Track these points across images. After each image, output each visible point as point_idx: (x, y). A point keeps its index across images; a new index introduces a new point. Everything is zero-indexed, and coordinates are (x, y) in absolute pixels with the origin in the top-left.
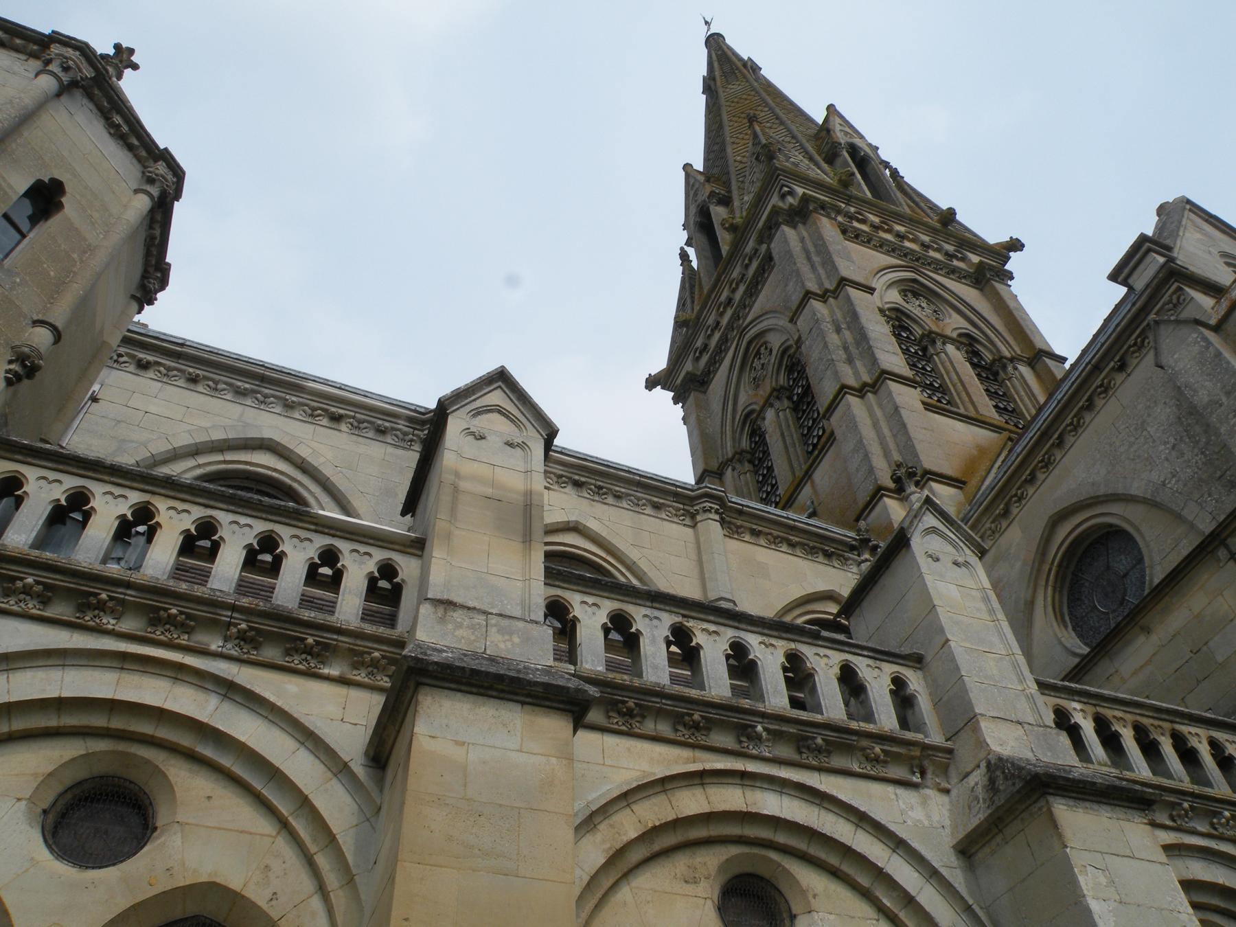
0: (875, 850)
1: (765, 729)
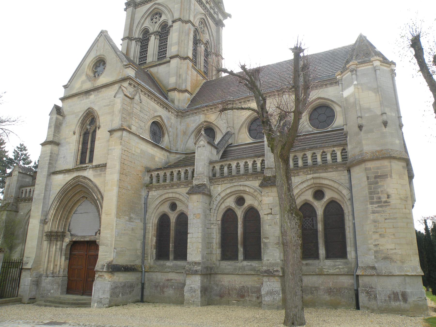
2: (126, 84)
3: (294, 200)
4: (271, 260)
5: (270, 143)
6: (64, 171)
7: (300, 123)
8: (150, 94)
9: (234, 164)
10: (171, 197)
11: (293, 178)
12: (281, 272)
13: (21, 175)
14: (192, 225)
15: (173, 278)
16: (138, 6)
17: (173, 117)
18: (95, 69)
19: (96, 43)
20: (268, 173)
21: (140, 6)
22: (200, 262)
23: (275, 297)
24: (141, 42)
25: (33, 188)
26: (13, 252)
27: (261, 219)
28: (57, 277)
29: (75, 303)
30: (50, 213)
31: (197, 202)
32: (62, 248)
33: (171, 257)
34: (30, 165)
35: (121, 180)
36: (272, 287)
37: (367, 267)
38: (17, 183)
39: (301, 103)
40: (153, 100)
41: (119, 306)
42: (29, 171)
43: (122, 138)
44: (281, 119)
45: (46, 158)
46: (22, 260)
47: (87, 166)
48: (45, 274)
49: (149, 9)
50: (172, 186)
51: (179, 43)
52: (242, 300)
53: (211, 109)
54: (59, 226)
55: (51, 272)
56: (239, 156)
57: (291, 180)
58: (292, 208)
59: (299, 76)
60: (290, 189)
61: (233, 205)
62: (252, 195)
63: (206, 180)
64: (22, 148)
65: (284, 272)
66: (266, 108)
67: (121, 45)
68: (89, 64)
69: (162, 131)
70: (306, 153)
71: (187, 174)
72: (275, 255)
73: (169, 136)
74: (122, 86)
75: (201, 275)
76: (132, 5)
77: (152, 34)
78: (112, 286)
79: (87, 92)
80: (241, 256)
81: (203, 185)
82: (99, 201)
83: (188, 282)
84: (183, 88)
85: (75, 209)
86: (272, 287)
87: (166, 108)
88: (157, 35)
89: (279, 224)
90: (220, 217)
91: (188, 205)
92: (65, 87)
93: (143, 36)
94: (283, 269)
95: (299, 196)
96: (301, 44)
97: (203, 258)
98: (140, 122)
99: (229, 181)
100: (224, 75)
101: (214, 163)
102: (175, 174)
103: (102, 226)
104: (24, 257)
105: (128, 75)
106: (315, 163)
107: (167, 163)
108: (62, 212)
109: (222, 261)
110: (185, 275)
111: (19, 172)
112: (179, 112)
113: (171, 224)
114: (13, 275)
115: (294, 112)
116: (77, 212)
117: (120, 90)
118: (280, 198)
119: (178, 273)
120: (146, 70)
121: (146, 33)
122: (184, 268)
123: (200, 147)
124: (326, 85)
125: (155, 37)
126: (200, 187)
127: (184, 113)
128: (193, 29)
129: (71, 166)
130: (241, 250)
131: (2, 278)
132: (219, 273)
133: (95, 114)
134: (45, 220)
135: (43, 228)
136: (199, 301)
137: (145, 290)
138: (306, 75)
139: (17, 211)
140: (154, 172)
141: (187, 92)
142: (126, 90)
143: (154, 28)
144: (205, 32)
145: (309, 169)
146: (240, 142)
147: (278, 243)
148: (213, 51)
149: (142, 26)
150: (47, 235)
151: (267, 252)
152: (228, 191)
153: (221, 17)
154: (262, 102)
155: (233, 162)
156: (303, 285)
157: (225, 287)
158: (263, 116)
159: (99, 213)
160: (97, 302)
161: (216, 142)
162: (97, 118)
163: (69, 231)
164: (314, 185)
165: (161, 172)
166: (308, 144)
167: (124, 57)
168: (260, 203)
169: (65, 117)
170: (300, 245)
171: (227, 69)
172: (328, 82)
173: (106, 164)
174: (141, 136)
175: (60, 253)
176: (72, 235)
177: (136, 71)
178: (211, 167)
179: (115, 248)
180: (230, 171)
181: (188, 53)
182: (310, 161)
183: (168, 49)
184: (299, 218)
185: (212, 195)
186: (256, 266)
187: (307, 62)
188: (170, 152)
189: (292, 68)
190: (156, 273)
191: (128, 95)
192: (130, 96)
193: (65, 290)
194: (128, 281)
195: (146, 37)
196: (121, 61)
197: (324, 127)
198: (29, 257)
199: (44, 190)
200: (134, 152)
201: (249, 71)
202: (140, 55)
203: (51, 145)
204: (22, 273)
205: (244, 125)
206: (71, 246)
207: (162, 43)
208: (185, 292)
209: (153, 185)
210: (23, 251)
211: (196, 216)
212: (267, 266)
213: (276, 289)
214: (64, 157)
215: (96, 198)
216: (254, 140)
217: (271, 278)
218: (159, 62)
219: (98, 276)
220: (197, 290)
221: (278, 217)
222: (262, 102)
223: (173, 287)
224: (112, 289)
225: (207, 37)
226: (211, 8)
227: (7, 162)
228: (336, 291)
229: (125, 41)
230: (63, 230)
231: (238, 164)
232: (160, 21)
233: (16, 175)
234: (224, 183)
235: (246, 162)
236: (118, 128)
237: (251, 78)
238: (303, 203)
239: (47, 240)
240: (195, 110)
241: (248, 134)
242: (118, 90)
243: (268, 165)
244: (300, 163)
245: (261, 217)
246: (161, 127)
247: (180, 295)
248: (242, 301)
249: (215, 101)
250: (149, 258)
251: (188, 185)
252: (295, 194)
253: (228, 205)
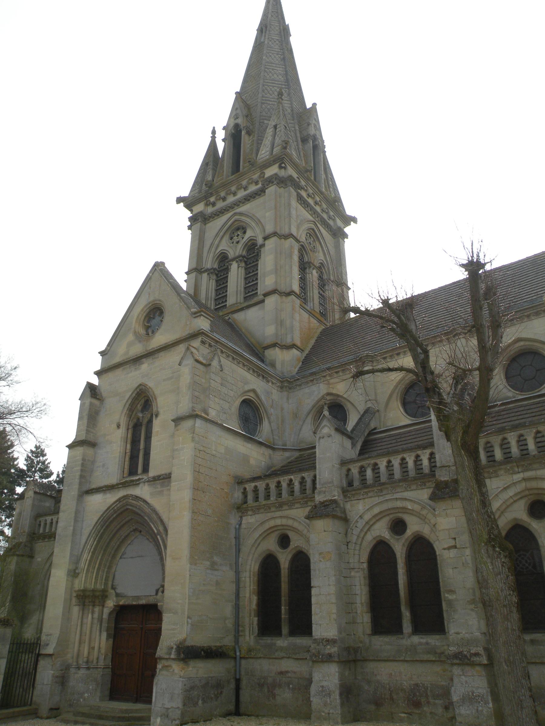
2: (196, 343)
3: (495, 521)
4: (464, 632)
5: (442, 425)
6: (104, 489)
7: (491, 386)
8: (235, 356)
9: (382, 464)
10: (280, 524)
11: (488, 481)
12: (484, 657)
13: (38, 497)
16: (209, 220)
17: (275, 391)
18: (148, 322)
19: (147, 283)
20: (443, 476)
21: (211, 220)
22: (336, 639)
23: (480, 708)
24: (217, 275)
25: (57, 516)
26: (26, 625)
27: (438, 557)
28: (95, 669)
29: (124, 717)
30: (83, 558)
31: (325, 531)
32: (102, 619)
33: (285, 630)
34: (50, 479)
35: (195, 500)
36: (472, 687)
38: (32, 511)
39: (489, 353)
40: (241, 365)
41: (198, 722)
42: (50, 490)
43: (194, 430)
44: (457, 382)
45: (75, 468)
46: (39, 638)
47: (139, 479)
48: (75, 664)
49: (226, 222)
50: (280, 506)
51: (276, 271)
53: (337, 372)
54: (97, 580)
55: (85, 660)
56: (390, 449)
57: (485, 486)
58: (492, 536)
59: (481, 308)
60: (485, 503)
61: (386, 535)
62: (418, 515)
63: (336, 494)
64: (39, 452)
65: (490, 657)
66: (429, 366)
67: (185, 281)
68: (139, 315)
69: (259, 415)
70: (506, 435)
71: (304, 484)
72: (471, 623)
73: (270, 423)
74: (190, 346)
75: (340, 662)
76: (200, 220)
77: (233, 260)
78: (185, 685)
79: (137, 360)
80: (407, 626)
81: (333, 502)
82: (161, 537)
83: (316, 677)
84: (288, 341)
85: (123, 550)
86: (472, 687)
87: (263, 377)
88: (241, 261)
89: (471, 565)
90: (365, 557)
91: (309, 537)
92: (102, 353)
93: (219, 265)
94: (487, 650)
95: (502, 512)
96: (478, 256)
97: (340, 632)
98: (222, 402)
99: (376, 492)
100: (352, 315)
101: (348, 463)
102: (284, 485)
103: (166, 579)
104: (43, 634)
105: (199, 329)
106: (525, 452)
107: (269, 468)
108: (102, 556)
109: (374, 637)
110: (311, 663)
111: (35, 493)
112: (284, 381)
113: (282, 572)
114: (25, 665)
115: (478, 369)
116: (125, 556)
117: (188, 353)
118: (469, 520)
120: (227, 318)
121: (223, 258)
122: (308, 651)
123: (323, 438)
124: (528, 316)
125: (238, 265)
126: (327, 505)
127: (292, 382)
128: (296, 246)
129: (114, 480)
130: (406, 614)
131: (9, 672)
132: (371, 658)
133: (150, 394)
134: (75, 570)
135: (73, 584)
136: (338, 713)
137: (242, 692)
138: (492, 304)
139: (31, 557)
140: (250, 484)
141: (296, 349)
142: (197, 353)
143: (236, 250)
144: (317, 249)
145: (515, 464)
146: (390, 424)
147: (473, 602)
148: (332, 278)
149: (216, 249)
150: (78, 596)
151: (454, 618)
152: (376, 510)
153: (339, 223)
154: (422, 356)
155: (381, 460)
156: (532, 685)
158: (426, 380)
159: (161, 557)
160: (161, 716)
161: (350, 426)
162: (154, 399)
163: (113, 588)
164: (527, 493)
165: (261, 483)
166: (509, 420)
167: (192, 300)
168: (434, 529)
169: (103, 401)
170: (516, 605)
171: (359, 308)
172: (530, 312)
173: (170, 474)
174: (224, 425)
175: (99, 626)
176: (117, 595)
177: (211, 320)
178: (344, 469)
179: (189, 617)
180: (377, 475)
181: (291, 286)
182: (515, 450)
183: (259, 281)
184: (507, 554)
185: (348, 517)
186: (437, 644)
187: (492, 283)
188: (273, 449)
189: (467, 295)
191: (201, 359)
192: (204, 362)
193: (107, 693)
194: (211, 675)
195: (224, 265)
196: (187, 306)
197: (533, 389)
198: (50, 635)
199: (73, 521)
200: (214, 452)
201: (395, 308)
202: (217, 295)
203: (83, 446)
204: (39, 663)
205: (395, 395)
206: (117, 614)
207: (250, 273)
208: (311, 695)
209: (249, 506)
210: (41, 623)
212: (458, 644)
213: (480, 691)
214: (104, 465)
215: (156, 531)
216: (413, 419)
217: (467, 668)
218: (246, 304)
219: (163, 667)
220: (334, 692)
221: (468, 552)
222: (422, 356)
223: (291, 686)
224: (186, 691)
225: (321, 256)
226: (323, 211)
227: (17, 475)
229: (191, 274)
230: (103, 587)
231: (389, 462)
232: (244, 240)
233: (31, 497)
234: (368, 496)
235: (403, 459)
236: (188, 414)
237: (399, 318)
238: (510, 526)
239: (79, 604)
240: (310, 376)
241: (402, 410)
242: (185, 353)
243: (441, 461)
244: (498, 455)
245: (437, 554)
246: (257, 409)
247: (303, 701)
249: (342, 359)
250: (247, 633)
251: (306, 503)
252: (494, 510)
253: (378, 534)
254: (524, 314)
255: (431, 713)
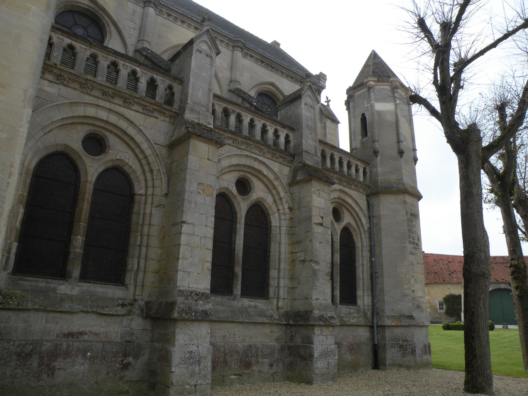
0: (131, 131)
1: (152, 108)
4: (321, 299)
14: (193, 205)
15: (88, 330)
31: (208, 159)
37: (401, 316)
52: (247, 372)
80: (238, 289)
119: (104, 315)
151: (316, 286)
155: (247, 114)
157: (219, 349)
172: (285, 72)
186: (263, 308)
190: (24, 315)
211: (203, 188)
220: (205, 358)
223: (89, 354)
228: (357, 348)
247: (108, 374)
248: (246, 374)
254: (282, 70)
255: (259, 371)
